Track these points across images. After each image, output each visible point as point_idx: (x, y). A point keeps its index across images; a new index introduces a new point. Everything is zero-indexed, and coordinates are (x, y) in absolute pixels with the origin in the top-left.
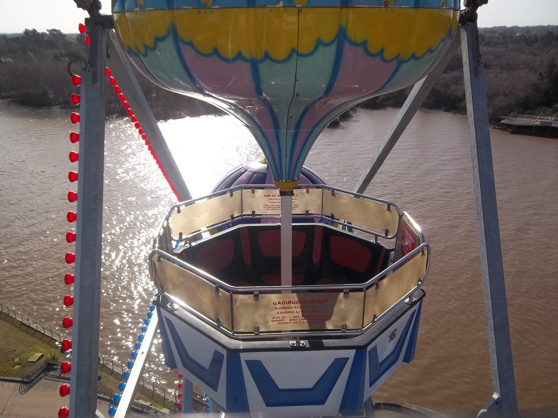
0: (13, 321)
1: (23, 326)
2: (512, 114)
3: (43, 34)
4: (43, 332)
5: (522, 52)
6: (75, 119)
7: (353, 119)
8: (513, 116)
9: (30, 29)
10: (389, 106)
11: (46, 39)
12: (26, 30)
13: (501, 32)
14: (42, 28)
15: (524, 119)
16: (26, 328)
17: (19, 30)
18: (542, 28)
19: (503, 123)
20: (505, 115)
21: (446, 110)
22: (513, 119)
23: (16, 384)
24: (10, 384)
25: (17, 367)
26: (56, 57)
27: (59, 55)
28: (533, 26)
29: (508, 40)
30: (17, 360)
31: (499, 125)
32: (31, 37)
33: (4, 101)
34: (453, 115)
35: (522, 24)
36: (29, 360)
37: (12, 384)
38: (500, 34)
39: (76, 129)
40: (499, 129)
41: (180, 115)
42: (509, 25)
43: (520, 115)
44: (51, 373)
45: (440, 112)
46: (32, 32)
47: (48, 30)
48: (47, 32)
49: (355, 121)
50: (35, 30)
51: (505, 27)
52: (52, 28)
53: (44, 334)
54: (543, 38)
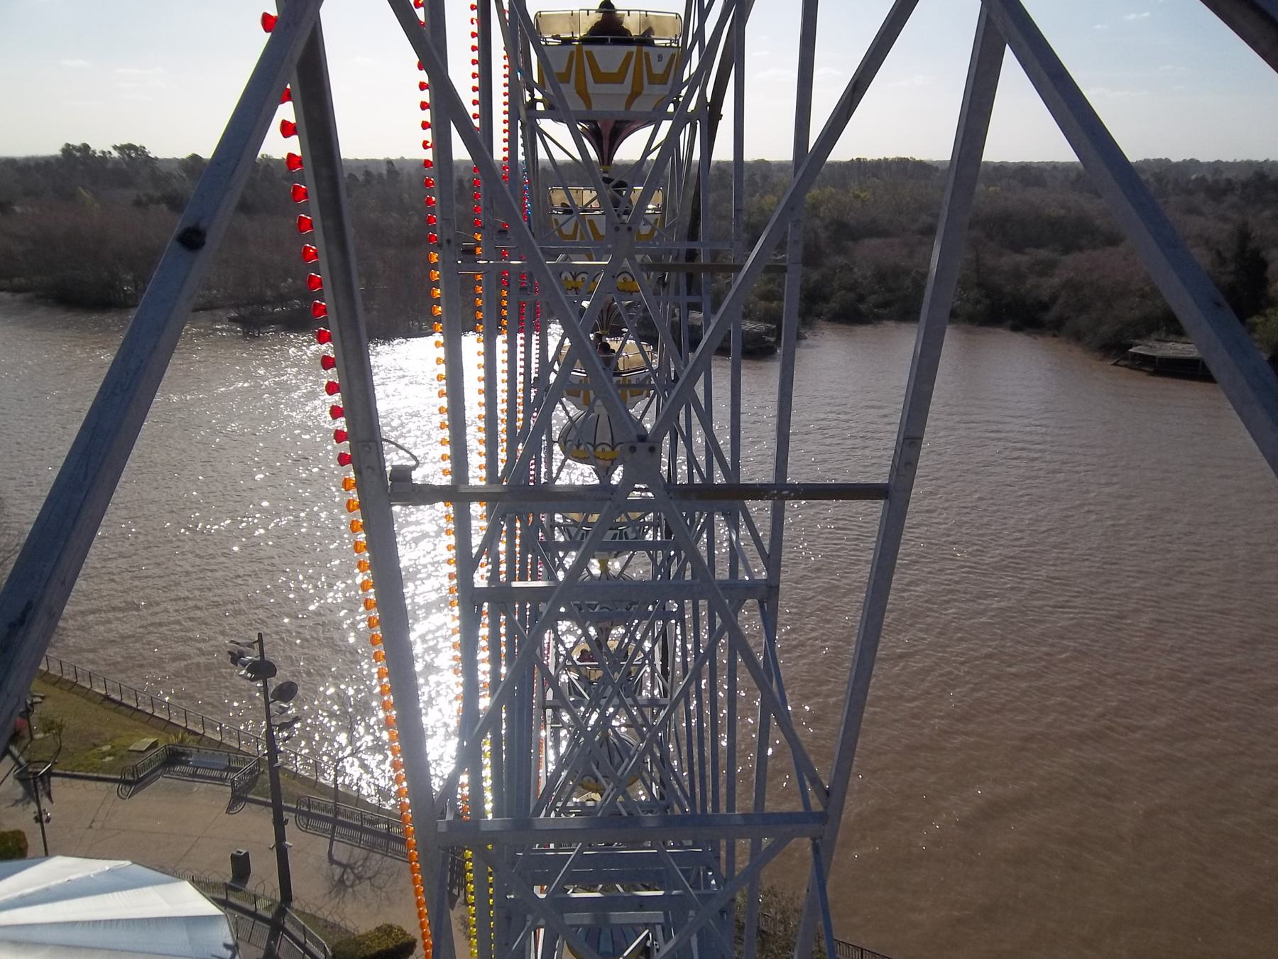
0: (87, 694)
1: (106, 703)
2: (1154, 336)
3: (104, 158)
4: (149, 711)
5: (1200, 213)
6: (322, 339)
7: (808, 341)
8: (1158, 340)
9: (77, 142)
10: (890, 318)
11: (110, 165)
12: (68, 145)
13: (1157, 170)
14: (103, 142)
15: (1180, 346)
16: (114, 706)
17: (50, 148)
18: (1249, 164)
19: (1135, 354)
20: (1139, 336)
21: (1016, 328)
22: (1157, 345)
23: (110, 785)
24: (99, 784)
25: (108, 759)
26: (138, 203)
27: (144, 199)
28: (1231, 160)
29: (1170, 187)
30: (106, 748)
31: (1126, 359)
32: (77, 160)
33: (19, 296)
34: (1028, 339)
35: (1207, 154)
36: (131, 748)
37: (103, 785)
38: (1154, 175)
39: (327, 349)
40: (1125, 366)
41: (420, 328)
42: (1176, 158)
43: (1172, 337)
44: (178, 769)
45: (1000, 330)
46: (79, 149)
47: (115, 147)
48: (115, 154)
49: (808, 346)
50: (86, 147)
51: (1168, 161)
52: (125, 142)
53: (152, 715)
54: (1245, 185)
